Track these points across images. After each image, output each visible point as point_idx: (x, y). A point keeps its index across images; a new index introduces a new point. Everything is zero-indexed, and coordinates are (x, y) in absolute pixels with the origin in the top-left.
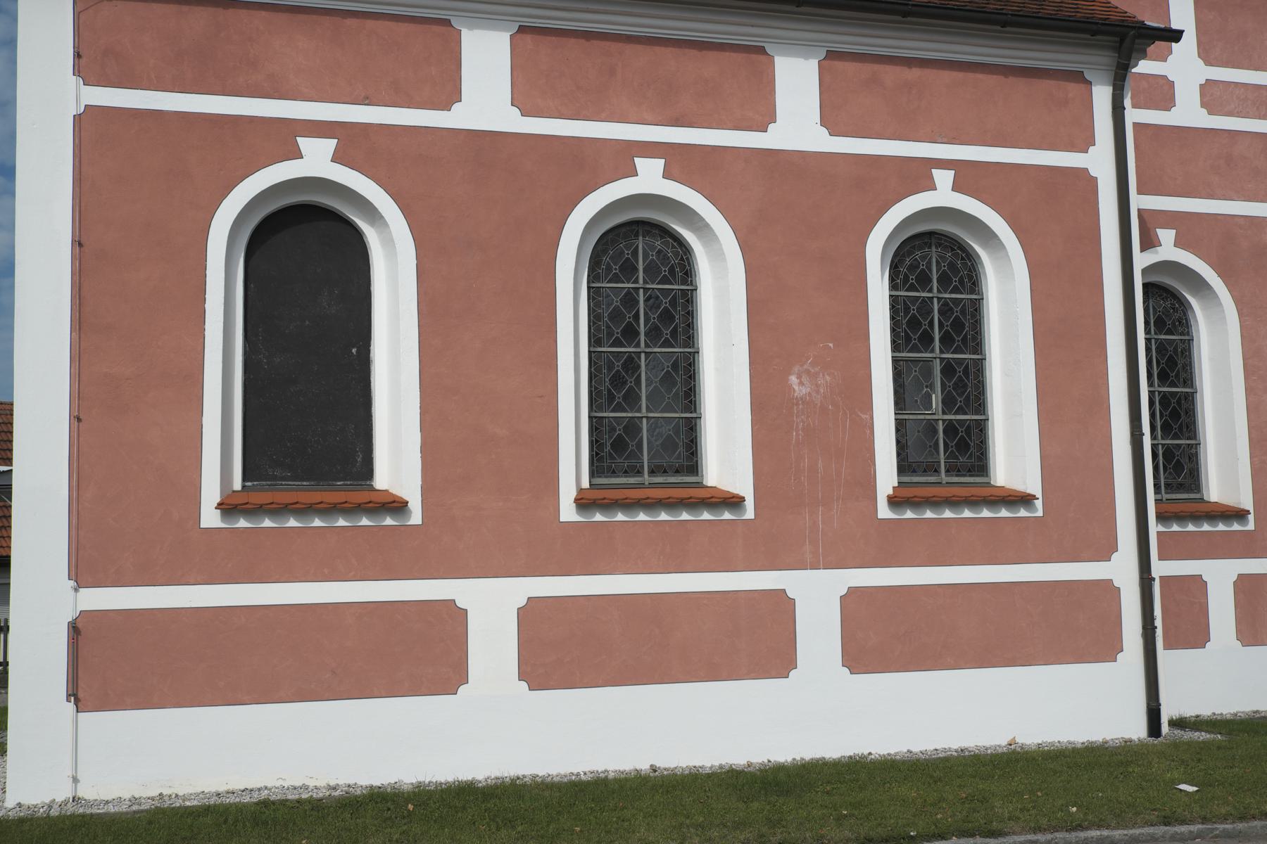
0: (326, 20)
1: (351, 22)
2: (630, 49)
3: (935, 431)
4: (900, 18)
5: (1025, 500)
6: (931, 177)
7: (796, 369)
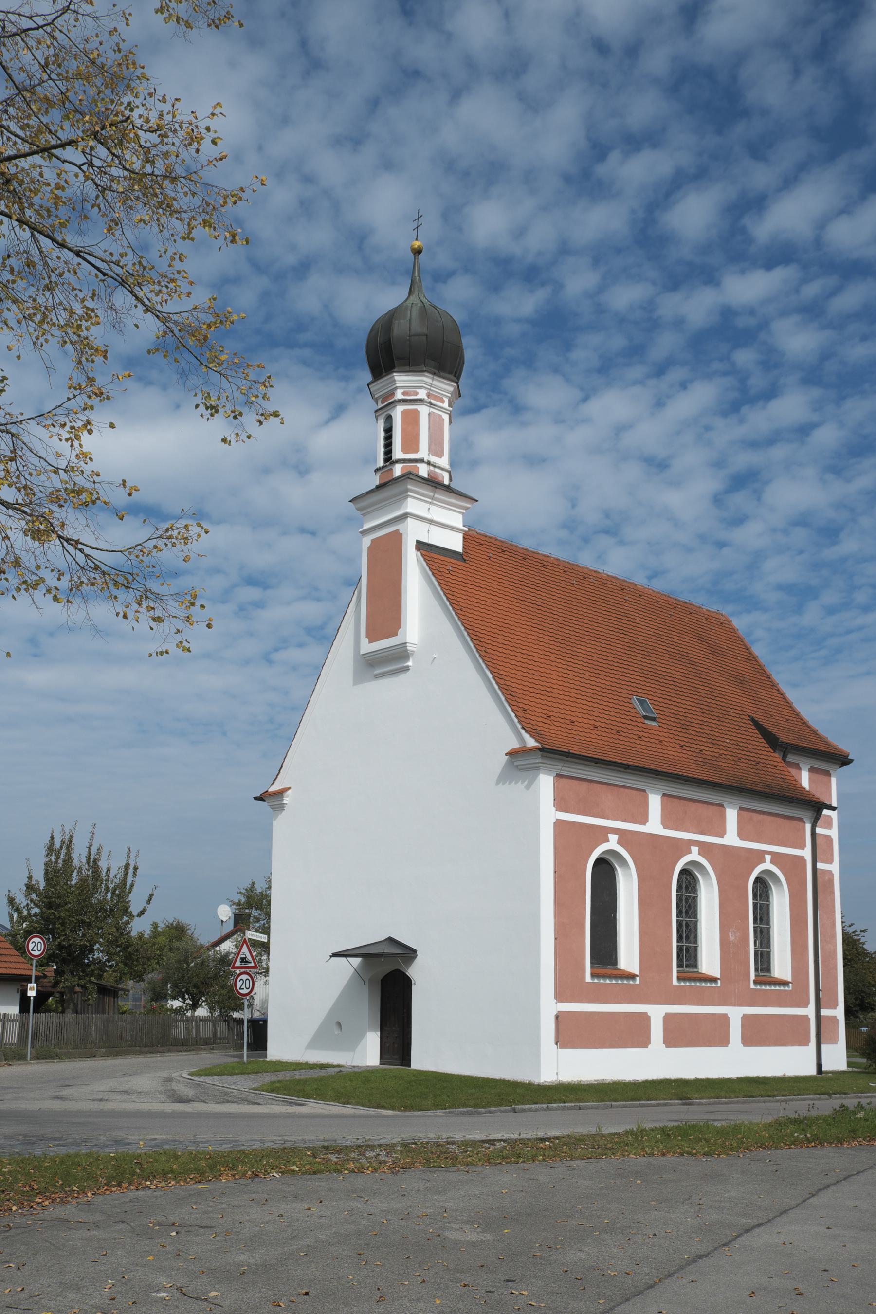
0: (616, 789)
1: (622, 790)
2: (690, 803)
3: (682, 950)
4: (593, 764)
5: (633, 977)
6: (764, 858)
7: (731, 930)
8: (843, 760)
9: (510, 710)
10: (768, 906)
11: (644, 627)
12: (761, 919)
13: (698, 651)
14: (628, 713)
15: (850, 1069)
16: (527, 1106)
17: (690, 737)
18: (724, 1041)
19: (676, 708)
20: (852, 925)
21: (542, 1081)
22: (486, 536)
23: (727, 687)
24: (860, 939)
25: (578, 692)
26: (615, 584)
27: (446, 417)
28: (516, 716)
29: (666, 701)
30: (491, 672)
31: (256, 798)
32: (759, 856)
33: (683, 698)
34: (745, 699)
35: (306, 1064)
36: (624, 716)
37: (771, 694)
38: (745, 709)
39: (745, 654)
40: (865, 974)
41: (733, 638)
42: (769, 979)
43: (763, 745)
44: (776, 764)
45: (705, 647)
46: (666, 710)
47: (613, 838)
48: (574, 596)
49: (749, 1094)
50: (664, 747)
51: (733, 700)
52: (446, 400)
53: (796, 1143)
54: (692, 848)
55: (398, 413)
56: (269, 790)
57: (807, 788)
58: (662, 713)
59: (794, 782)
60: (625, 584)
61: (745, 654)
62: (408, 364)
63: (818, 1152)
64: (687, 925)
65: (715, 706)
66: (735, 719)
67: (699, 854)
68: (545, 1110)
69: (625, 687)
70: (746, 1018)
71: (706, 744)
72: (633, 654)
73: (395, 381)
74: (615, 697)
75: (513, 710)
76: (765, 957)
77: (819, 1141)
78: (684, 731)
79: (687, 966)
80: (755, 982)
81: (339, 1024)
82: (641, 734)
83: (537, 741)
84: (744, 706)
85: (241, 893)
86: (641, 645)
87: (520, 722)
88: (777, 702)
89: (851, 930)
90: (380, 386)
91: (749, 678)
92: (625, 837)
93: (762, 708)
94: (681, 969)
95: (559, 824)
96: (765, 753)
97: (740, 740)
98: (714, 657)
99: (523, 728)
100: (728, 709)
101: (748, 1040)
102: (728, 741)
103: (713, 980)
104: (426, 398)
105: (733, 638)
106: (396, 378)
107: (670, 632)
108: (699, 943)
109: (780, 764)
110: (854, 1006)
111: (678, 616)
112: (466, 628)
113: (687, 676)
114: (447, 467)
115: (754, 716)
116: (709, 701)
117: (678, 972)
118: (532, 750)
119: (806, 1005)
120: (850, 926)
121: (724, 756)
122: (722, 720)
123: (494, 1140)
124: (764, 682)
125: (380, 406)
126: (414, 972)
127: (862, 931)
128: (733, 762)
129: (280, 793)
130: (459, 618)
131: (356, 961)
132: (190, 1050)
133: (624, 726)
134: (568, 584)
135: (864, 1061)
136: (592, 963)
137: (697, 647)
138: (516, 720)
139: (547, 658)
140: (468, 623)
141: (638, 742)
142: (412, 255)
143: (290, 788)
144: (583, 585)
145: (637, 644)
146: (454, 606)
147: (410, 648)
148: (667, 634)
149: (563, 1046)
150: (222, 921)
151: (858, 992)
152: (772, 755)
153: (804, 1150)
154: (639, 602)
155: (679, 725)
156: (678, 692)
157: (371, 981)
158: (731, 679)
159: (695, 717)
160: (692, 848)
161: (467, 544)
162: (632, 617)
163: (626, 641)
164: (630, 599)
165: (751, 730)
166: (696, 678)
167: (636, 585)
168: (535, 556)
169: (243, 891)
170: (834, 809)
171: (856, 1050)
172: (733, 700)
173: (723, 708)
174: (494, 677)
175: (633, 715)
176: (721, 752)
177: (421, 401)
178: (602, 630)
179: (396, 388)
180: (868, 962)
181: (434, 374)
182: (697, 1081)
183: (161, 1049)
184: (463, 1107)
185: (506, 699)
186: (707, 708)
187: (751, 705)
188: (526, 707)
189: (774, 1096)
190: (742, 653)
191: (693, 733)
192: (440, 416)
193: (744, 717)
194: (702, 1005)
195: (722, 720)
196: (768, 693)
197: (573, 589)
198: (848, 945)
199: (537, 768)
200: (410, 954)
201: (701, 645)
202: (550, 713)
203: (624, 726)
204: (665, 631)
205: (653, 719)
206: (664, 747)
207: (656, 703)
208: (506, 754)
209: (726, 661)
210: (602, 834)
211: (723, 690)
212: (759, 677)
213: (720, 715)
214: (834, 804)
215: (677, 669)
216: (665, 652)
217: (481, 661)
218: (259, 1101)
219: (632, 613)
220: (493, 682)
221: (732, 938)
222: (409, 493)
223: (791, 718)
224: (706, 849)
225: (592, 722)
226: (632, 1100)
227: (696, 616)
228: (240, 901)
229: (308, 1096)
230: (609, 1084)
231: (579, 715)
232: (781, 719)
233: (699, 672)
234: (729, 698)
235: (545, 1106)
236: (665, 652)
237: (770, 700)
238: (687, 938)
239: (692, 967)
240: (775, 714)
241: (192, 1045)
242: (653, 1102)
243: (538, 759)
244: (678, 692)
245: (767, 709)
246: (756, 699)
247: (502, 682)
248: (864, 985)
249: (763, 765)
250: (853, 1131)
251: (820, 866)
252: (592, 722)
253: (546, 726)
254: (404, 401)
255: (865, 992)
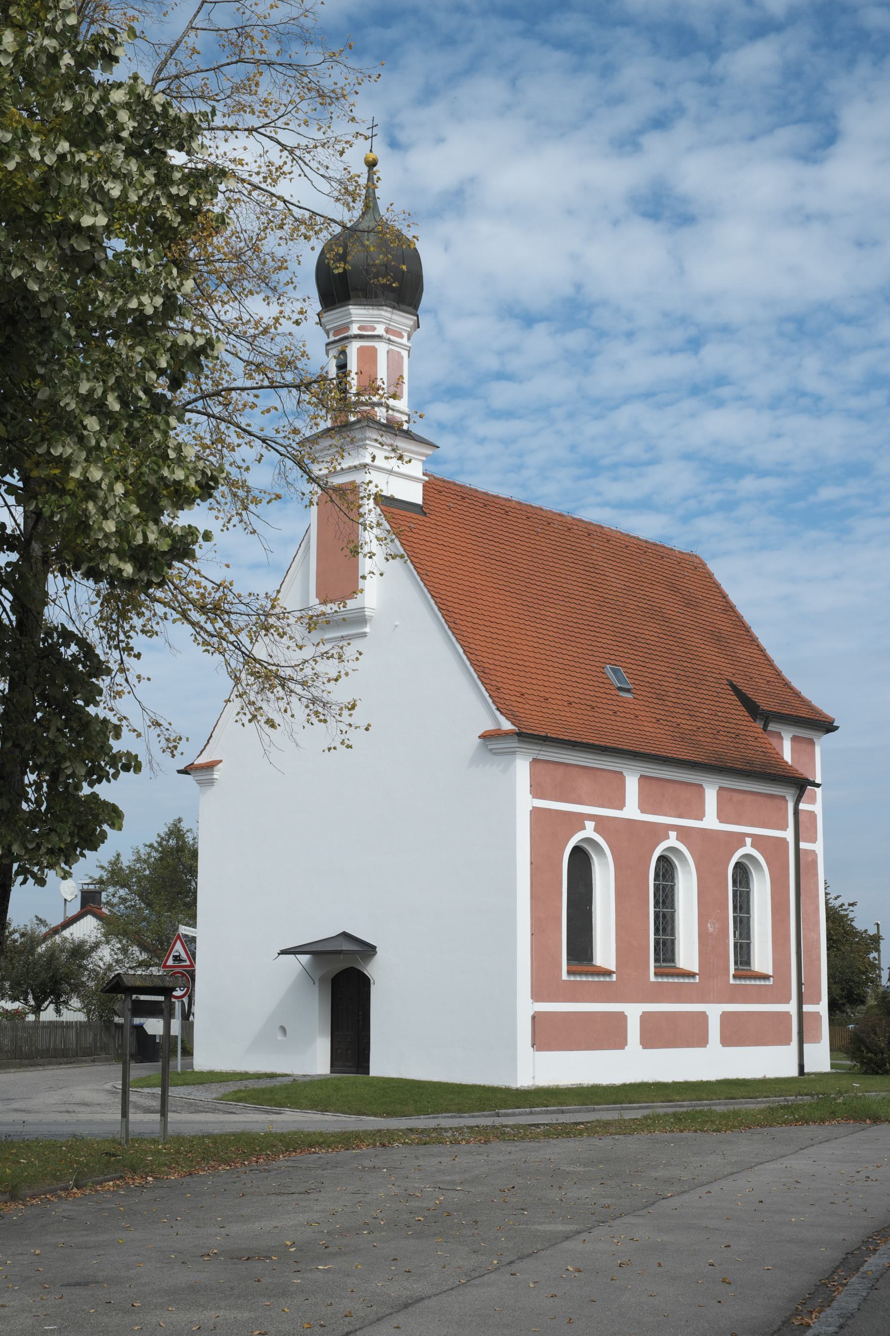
1: (598, 773)
5: (609, 973)
8: (827, 726)
9: (483, 689)
10: (748, 893)
11: (614, 580)
12: (741, 908)
13: (671, 604)
14: (602, 685)
15: (834, 1071)
16: (510, 1111)
17: (666, 708)
18: (702, 1041)
19: (650, 676)
20: (838, 897)
21: (519, 1086)
22: (444, 481)
23: (703, 646)
24: (847, 915)
25: (550, 663)
26: (581, 529)
27: (405, 354)
28: (490, 696)
29: (640, 668)
30: (462, 646)
31: (179, 772)
32: (739, 840)
33: (658, 663)
34: (723, 660)
35: (246, 1073)
36: (597, 689)
37: (751, 650)
38: (723, 672)
39: (722, 603)
40: (854, 958)
41: (709, 584)
42: (749, 973)
43: (742, 713)
44: (756, 735)
45: (678, 599)
46: (641, 678)
47: (590, 825)
48: (539, 547)
49: (730, 1096)
50: (640, 723)
51: (710, 661)
52: (405, 335)
53: (786, 1122)
54: (670, 833)
55: (353, 348)
56: (196, 763)
57: (790, 762)
58: (637, 682)
59: (776, 756)
60: (591, 527)
61: (722, 603)
62: (365, 296)
63: (805, 1128)
64: (664, 916)
65: (691, 670)
66: (713, 684)
67: (677, 839)
68: (528, 1114)
69: (597, 654)
70: (725, 1016)
71: (683, 716)
72: (604, 613)
73: (350, 314)
74: (588, 667)
75: (486, 689)
76: (745, 949)
77: (805, 1121)
78: (660, 702)
79: (664, 961)
80: (735, 977)
81: (283, 1029)
82: (616, 708)
83: (513, 723)
84: (722, 668)
85: (102, 867)
86: (612, 602)
87: (494, 702)
88: (757, 660)
89: (837, 903)
90: (334, 317)
91: (726, 633)
92: (602, 824)
93: (741, 668)
94: (658, 964)
95: (536, 813)
96: (744, 723)
97: (718, 709)
98: (689, 610)
99: (498, 709)
100: (705, 673)
101: (726, 1041)
102: (706, 711)
103: (692, 975)
104: (385, 334)
105: (709, 584)
106: (352, 311)
107: (641, 583)
108: (677, 935)
109: (761, 735)
110: (841, 998)
111: (649, 562)
112: (433, 596)
113: (661, 636)
114: (407, 410)
115: (732, 679)
116: (685, 664)
117: (655, 967)
118: (507, 734)
119: (787, 1000)
120: (836, 899)
121: (702, 729)
122: (699, 686)
123: (538, 1124)
124: (743, 637)
125: (332, 338)
126: (375, 970)
127: (850, 905)
128: (711, 736)
129: (210, 766)
130: (425, 584)
131: (305, 958)
132: (71, 1063)
133: (598, 700)
134: (533, 532)
135: (849, 1063)
136: (568, 960)
137: (671, 600)
138: (490, 701)
139: (516, 625)
140: (435, 590)
141: (613, 718)
142: (366, 169)
143: (221, 761)
144: (548, 532)
145: (607, 601)
146: (419, 570)
147: (368, 613)
148: (638, 587)
149: (539, 1049)
150: (65, 900)
151: (845, 981)
152: (753, 724)
153: (793, 1127)
154: (607, 549)
155: (654, 696)
156: (652, 656)
157: (322, 979)
158: (708, 635)
159: (671, 685)
160: (670, 833)
161: (426, 497)
162: (601, 568)
163: (596, 598)
164: (598, 546)
165: (730, 697)
166: (671, 638)
167: (603, 527)
168: (496, 500)
169: (106, 865)
170: (818, 786)
171: (840, 1050)
172: (710, 661)
173: (700, 672)
174: (465, 651)
175: (607, 686)
176: (699, 724)
177: (379, 337)
178: (569, 587)
179: (352, 322)
180: (857, 943)
181: (394, 308)
182: (675, 1084)
183: (41, 1061)
184: (446, 1112)
185: (479, 677)
186: (682, 673)
187: (729, 666)
188: (499, 685)
189: (756, 1098)
190: (718, 602)
191: (670, 704)
192: (399, 353)
193: (722, 681)
194: (680, 1002)
195: (699, 686)
196: (746, 649)
197: (538, 538)
198: (833, 922)
199: (514, 753)
200: (369, 950)
201: (674, 597)
202: (524, 691)
203: (598, 700)
204: (636, 582)
205: (628, 691)
206: (640, 723)
207: (630, 671)
208: (479, 737)
209: (701, 613)
210: (578, 820)
211: (699, 650)
212: (737, 631)
213: (697, 681)
214: (818, 781)
215: (650, 629)
216: (636, 608)
217: (450, 633)
218: (234, 1110)
219: (601, 564)
220: (465, 657)
221: (711, 930)
222: (368, 442)
223: (772, 680)
224: (684, 834)
225: (566, 698)
226: (614, 1103)
227: (668, 560)
228: (101, 878)
229: (281, 1105)
230: (587, 1087)
231: (553, 691)
232: (761, 681)
233: (673, 630)
234: (706, 660)
235: (528, 1110)
236: (636, 608)
237: (749, 658)
238: (664, 930)
239: (669, 961)
240: (756, 676)
241: (73, 1056)
242: (634, 1105)
243: (514, 743)
244: (652, 656)
245: (746, 669)
246: (734, 658)
247: (473, 657)
248: (853, 972)
249: (743, 737)
250: (833, 1113)
251: (803, 845)
252: (566, 698)
253: (521, 705)
254: (361, 337)
255: (853, 981)
